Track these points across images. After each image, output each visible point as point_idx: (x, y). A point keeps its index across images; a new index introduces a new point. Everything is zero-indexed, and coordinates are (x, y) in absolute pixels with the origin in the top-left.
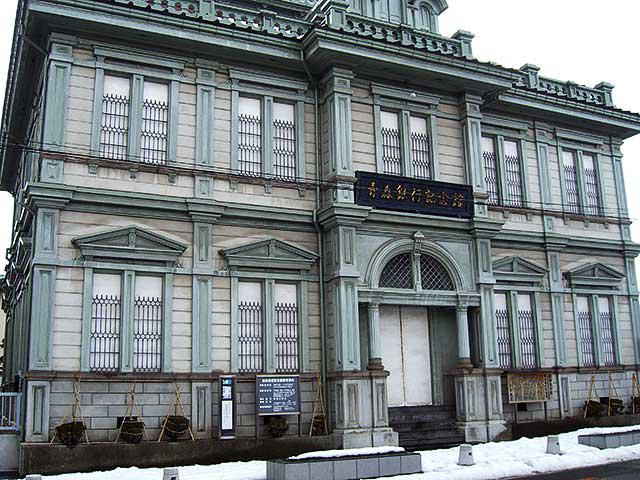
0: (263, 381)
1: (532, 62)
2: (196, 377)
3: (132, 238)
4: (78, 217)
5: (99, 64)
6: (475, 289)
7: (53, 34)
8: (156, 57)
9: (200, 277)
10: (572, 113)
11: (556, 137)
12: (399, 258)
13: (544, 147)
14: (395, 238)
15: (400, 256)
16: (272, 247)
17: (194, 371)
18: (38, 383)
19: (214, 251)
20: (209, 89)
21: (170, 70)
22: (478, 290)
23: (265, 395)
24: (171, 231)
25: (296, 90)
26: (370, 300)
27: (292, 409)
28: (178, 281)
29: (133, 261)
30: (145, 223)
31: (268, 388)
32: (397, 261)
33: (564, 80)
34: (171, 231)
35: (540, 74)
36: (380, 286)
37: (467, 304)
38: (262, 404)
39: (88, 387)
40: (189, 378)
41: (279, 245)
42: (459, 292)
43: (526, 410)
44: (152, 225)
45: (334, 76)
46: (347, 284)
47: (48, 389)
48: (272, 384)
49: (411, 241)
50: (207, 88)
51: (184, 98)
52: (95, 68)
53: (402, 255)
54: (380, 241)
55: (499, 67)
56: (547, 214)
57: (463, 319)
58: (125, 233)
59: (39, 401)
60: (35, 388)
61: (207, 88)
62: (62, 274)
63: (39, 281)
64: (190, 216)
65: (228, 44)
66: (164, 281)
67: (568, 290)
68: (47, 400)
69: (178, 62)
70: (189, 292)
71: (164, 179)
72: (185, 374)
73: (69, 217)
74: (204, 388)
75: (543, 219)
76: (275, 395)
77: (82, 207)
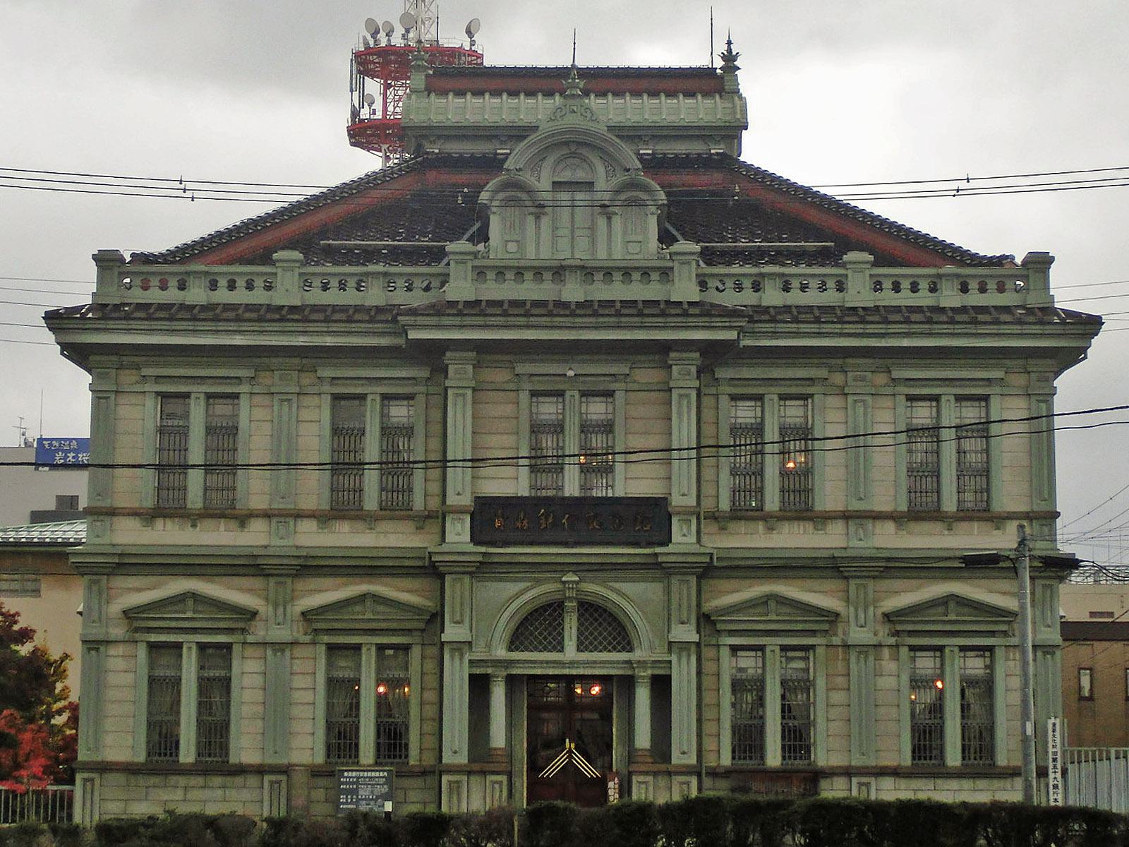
0: (346, 774)
4: (132, 582)
5: (147, 387)
6: (666, 650)
7: (448, 354)
8: (194, 365)
12: (596, 610)
14: (538, 582)
18: (86, 775)
20: (290, 397)
22: (670, 651)
23: (347, 792)
24: (821, 596)
26: (489, 671)
28: (250, 651)
29: (195, 630)
31: (353, 783)
32: (541, 615)
34: (821, 596)
36: (579, 650)
37: (649, 672)
38: (343, 803)
39: (142, 780)
40: (260, 770)
41: (377, 599)
42: (637, 655)
44: (386, 585)
46: (453, 650)
47: (97, 782)
50: (285, 397)
51: (259, 413)
54: (512, 588)
57: (643, 696)
58: (181, 599)
59: (88, 796)
60: (85, 780)
61: (285, 397)
62: (112, 651)
66: (942, 658)
67: (892, 640)
68: (96, 793)
69: (818, 366)
70: (716, 666)
71: (233, 524)
73: (120, 582)
74: (279, 782)
76: (361, 792)
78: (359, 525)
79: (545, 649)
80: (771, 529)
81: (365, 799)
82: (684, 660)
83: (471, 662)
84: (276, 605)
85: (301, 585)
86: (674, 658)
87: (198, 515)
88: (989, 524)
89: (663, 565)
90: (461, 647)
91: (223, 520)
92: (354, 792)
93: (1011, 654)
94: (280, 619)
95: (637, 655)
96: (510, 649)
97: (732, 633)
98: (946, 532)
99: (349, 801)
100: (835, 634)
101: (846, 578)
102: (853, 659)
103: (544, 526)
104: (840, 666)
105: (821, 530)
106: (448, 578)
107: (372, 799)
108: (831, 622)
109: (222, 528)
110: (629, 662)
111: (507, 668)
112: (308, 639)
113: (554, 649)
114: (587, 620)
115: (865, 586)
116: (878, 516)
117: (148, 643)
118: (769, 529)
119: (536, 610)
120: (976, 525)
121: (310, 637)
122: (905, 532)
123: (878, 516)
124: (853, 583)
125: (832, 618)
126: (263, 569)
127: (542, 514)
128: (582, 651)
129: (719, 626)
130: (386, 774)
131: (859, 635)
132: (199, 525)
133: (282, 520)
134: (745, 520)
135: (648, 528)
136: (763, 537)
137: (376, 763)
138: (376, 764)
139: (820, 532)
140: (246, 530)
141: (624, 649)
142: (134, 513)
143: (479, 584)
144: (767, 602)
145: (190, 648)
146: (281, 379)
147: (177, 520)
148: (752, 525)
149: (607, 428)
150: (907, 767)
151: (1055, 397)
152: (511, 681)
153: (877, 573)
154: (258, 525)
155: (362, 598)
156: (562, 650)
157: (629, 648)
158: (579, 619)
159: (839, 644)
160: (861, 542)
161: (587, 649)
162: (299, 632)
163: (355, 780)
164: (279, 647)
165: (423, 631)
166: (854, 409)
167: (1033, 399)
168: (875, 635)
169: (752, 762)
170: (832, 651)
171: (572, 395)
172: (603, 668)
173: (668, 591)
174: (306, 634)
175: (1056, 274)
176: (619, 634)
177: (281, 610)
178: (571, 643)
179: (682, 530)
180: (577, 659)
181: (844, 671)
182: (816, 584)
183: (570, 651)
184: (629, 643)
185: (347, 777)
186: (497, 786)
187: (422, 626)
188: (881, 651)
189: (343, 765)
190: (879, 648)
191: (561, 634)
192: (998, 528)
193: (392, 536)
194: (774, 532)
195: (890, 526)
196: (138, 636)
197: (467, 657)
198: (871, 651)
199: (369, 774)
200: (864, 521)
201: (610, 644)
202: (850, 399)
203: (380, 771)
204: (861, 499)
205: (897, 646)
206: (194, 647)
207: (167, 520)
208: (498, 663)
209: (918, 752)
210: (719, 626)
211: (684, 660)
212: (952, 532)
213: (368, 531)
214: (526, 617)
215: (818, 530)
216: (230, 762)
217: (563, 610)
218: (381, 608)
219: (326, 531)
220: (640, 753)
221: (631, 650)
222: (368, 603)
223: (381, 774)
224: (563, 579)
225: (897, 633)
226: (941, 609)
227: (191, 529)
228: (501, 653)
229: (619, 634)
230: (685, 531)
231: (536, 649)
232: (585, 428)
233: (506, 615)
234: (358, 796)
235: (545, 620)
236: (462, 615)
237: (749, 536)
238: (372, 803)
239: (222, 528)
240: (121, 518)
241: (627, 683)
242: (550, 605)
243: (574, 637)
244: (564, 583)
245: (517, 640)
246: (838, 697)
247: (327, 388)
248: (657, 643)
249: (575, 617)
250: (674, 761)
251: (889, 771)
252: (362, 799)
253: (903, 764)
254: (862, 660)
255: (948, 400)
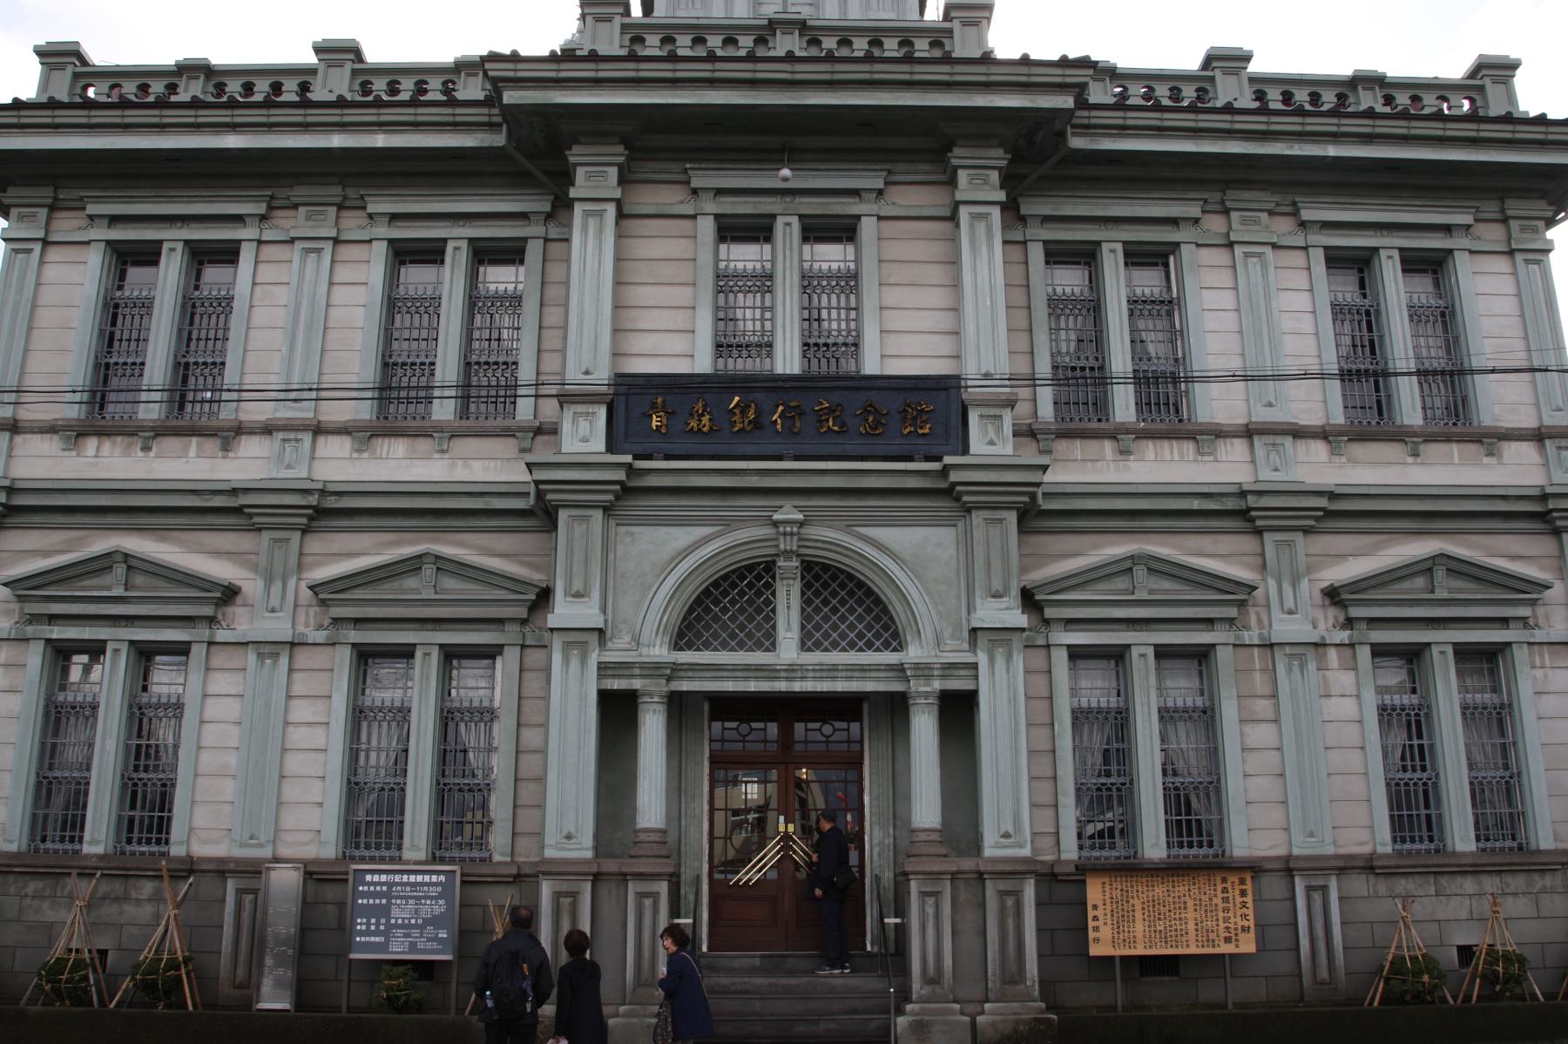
0: (368, 878)
1: (1228, 40)
2: (1301, 864)
3: (1440, 574)
9: (1288, 650)
10: (1332, 151)
11: (1303, 224)
12: (834, 577)
13: (1259, 255)
15: (742, 572)
16: (1440, 574)
17: (1296, 851)
19: (1310, 590)
21: (238, 219)
23: (369, 911)
25: (523, 216)
26: (637, 684)
27: (435, 945)
30: (1163, 545)
32: (733, 586)
33: (1345, 70)
35: (1254, 67)
36: (804, 647)
37: (937, 685)
41: (444, 565)
42: (914, 653)
43: (1177, 973)
45: (576, 165)
46: (567, 646)
48: (390, 885)
49: (767, 531)
52: (1305, 248)
53: (750, 568)
54: (683, 536)
55: (515, 57)
56: (1551, 437)
57: (924, 728)
63: (405, 660)
64: (1252, 520)
65: (337, 141)
67: (1343, 636)
71: (212, 445)
72: (1278, 858)
75: (1252, 445)
76: (395, 912)
77: (37, 519)
78: (423, 445)
79: (741, 646)
80: (1124, 452)
81: (403, 926)
82: (1000, 661)
83: (602, 667)
84: (269, 581)
85: (316, 544)
86: (982, 658)
87: (152, 429)
88: (1472, 447)
89: (246, 510)
90: (578, 637)
91: (194, 440)
92: (385, 911)
93: (1537, 658)
94: (275, 601)
95: (914, 653)
96: (677, 647)
97: (1070, 623)
98: (1410, 460)
99: (373, 928)
100: (1247, 627)
101: (1259, 532)
102: (1281, 667)
103: (738, 426)
104: (1259, 681)
105: (1210, 454)
106: (563, 515)
107: (416, 926)
108: (1242, 604)
109: (193, 452)
110: (900, 669)
111: (669, 679)
112: (321, 636)
113: (759, 646)
114: (817, 594)
115: (1290, 544)
116: (1299, 433)
117: (48, 641)
118: (1122, 452)
119: (725, 577)
120: (1455, 448)
121: (325, 633)
122: (1344, 459)
123: (1299, 433)
124: (1269, 538)
125: (1239, 594)
126: (251, 516)
127: (737, 405)
128: (809, 650)
129: (1050, 612)
130: (442, 878)
131: (1287, 628)
132: (154, 449)
133: (292, 435)
134: (1083, 437)
135: (927, 431)
136: (1112, 466)
137: (434, 858)
138: (434, 859)
139: (1206, 458)
140: (231, 454)
141: (887, 645)
142: (51, 429)
143: (622, 529)
144: (1131, 569)
145: (116, 651)
146: (308, 218)
147: (119, 439)
148: (1093, 445)
149: (849, 281)
150: (1387, 856)
151: (1551, 255)
152: (680, 707)
153: (1311, 522)
154: (251, 447)
155: (413, 565)
156: (772, 647)
157: (895, 640)
158: (803, 594)
159: (1256, 642)
160: (1277, 473)
161: (818, 645)
162: (307, 625)
163: (385, 888)
164: (268, 649)
165: (524, 622)
166: (1246, 265)
167: (1519, 257)
168: (1315, 627)
169: (1114, 853)
170: (1242, 652)
171: (787, 229)
172: (850, 678)
173: (967, 545)
174: (320, 627)
175: (1520, 80)
176: (878, 619)
177: (276, 588)
178: (789, 635)
179: (987, 433)
180: (799, 662)
181: (1267, 691)
182: (1205, 542)
183: (788, 649)
184: (896, 635)
185: (369, 884)
186: (648, 902)
187: (522, 612)
188: (1326, 653)
189: (362, 860)
190: (1321, 650)
191: (770, 618)
192: (1491, 454)
193: (477, 464)
194: (1132, 458)
195: (1319, 449)
196: (30, 630)
197: (594, 658)
198: (1311, 654)
199: (412, 878)
200: (1279, 439)
201: (860, 636)
202: (1238, 250)
203: (431, 872)
204: (1270, 405)
205: (1352, 645)
206: (124, 648)
207: (105, 439)
208: (653, 669)
209: (1401, 825)
210: (1050, 612)
211: (1000, 661)
212: (1419, 460)
213: (436, 455)
214: (707, 589)
215: (1202, 454)
216: (171, 854)
217: (773, 578)
218: (449, 583)
219: (366, 455)
220: (923, 836)
221: (900, 647)
222: (428, 571)
223: (434, 878)
224: (776, 517)
225: (1349, 623)
226: (1420, 582)
227: (140, 454)
228: (660, 652)
229: (878, 619)
230: (992, 435)
231: (724, 646)
232: (810, 282)
233: (671, 581)
234: (388, 919)
235: (742, 594)
236: (586, 582)
237: (1089, 464)
238: (415, 933)
239: (193, 452)
240: (28, 436)
241: (895, 708)
242: (750, 568)
243: (796, 627)
244: (775, 524)
245: (687, 633)
246: (1262, 734)
247: (384, 231)
248: (947, 633)
249: (796, 588)
250: (988, 852)
251: (1360, 863)
252: (397, 926)
253: (1380, 850)
254: (1296, 669)
255: (1390, 257)
